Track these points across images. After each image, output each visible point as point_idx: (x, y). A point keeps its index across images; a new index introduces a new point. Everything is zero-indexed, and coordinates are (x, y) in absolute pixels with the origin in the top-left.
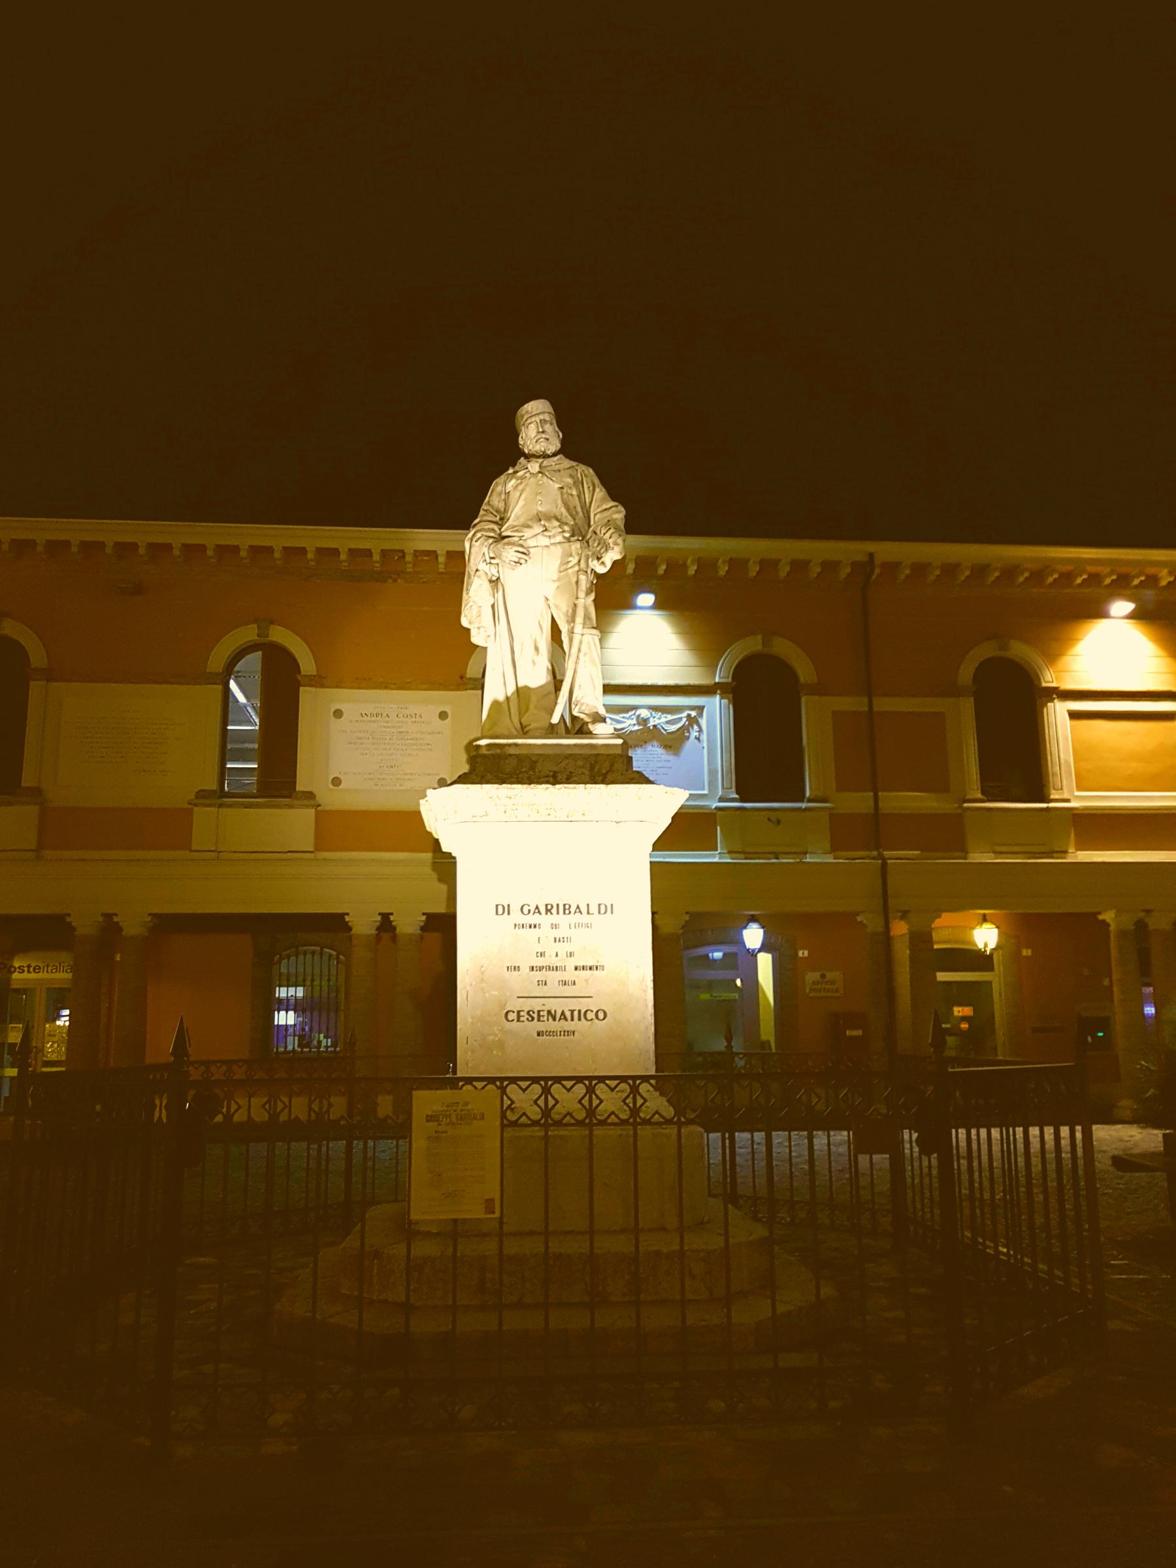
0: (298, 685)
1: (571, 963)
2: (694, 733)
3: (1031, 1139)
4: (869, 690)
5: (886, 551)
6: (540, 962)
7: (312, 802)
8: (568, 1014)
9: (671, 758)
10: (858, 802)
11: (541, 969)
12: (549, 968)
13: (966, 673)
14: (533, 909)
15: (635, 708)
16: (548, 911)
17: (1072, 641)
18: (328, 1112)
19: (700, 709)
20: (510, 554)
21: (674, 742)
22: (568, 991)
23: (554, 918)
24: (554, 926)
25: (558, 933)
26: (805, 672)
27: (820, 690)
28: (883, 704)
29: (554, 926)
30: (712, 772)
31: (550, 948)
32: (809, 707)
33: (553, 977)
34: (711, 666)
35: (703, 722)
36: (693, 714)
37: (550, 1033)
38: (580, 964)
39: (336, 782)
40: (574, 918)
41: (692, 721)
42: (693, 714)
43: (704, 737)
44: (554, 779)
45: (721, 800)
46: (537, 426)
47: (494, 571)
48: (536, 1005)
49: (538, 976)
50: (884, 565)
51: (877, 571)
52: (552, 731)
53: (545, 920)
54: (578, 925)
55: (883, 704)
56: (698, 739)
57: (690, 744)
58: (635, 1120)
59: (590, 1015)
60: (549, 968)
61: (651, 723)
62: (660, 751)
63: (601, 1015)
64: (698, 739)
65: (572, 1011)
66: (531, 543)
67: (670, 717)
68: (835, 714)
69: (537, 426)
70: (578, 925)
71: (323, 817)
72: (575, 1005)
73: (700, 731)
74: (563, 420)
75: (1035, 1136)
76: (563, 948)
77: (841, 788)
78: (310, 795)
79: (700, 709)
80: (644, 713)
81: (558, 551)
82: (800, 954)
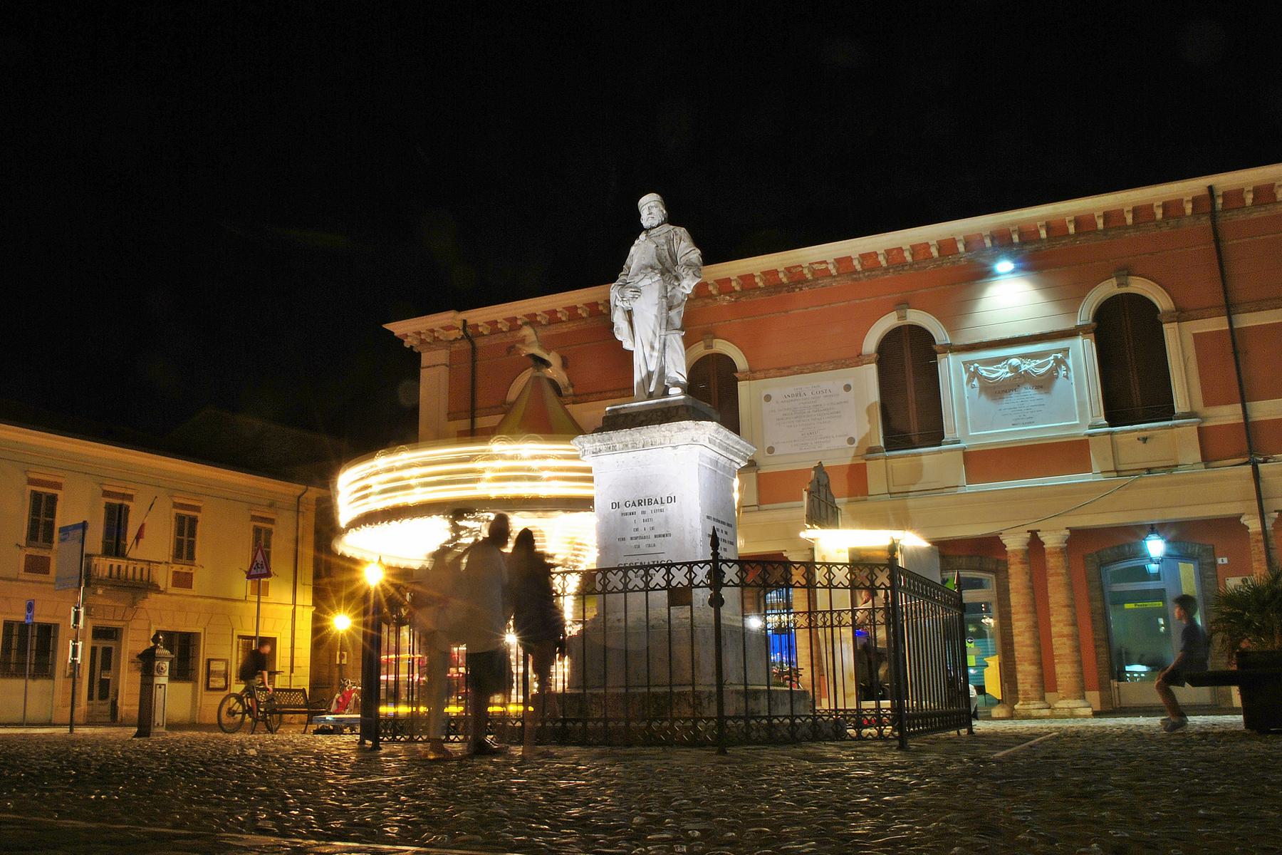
0: (737, 380)
1: (652, 534)
2: (1062, 373)
4: (1230, 309)
5: (1225, 181)
6: (636, 534)
9: (1044, 396)
10: (1228, 414)
12: (641, 538)
15: (1007, 358)
17: (982, 290)
19: (1066, 350)
20: (629, 294)
21: (1044, 383)
22: (652, 550)
23: (643, 508)
24: (643, 513)
25: (645, 517)
26: (1162, 301)
27: (1181, 314)
28: (1247, 320)
29: (643, 513)
30: (1081, 404)
31: (642, 526)
32: (1170, 332)
33: (643, 543)
34: (1073, 311)
35: (1070, 362)
36: (1060, 355)
39: (771, 450)
41: (1059, 362)
42: (1060, 355)
43: (1072, 374)
44: (641, 424)
45: (1091, 427)
46: (650, 208)
47: (626, 305)
49: (634, 542)
50: (1226, 195)
51: (1220, 201)
52: (651, 396)
53: (639, 509)
55: (1247, 320)
56: (1066, 377)
57: (1059, 383)
60: (641, 538)
61: (1023, 368)
62: (1032, 392)
64: (1066, 377)
66: (641, 284)
67: (1039, 362)
68: (1197, 337)
69: (650, 208)
70: (656, 511)
73: (1068, 369)
74: (668, 203)
75: (1021, 634)
77: (1209, 402)
79: (1066, 350)
80: (1015, 362)
81: (657, 286)
82: (1220, 561)
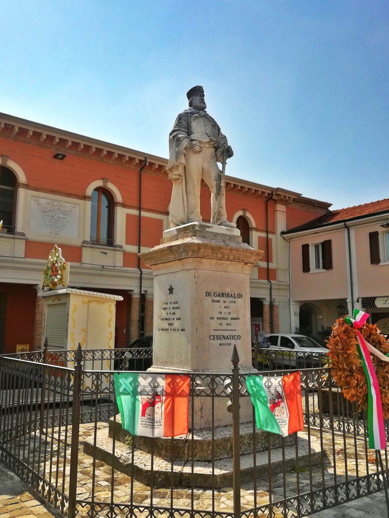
1: (229, 317)
3: (46, 474)
4: (140, 209)
7: (122, 249)
8: (229, 337)
11: (220, 318)
13: (90, 190)
14: (218, 294)
16: (223, 296)
18: (101, 385)
24: (224, 302)
25: (225, 305)
26: (22, 177)
28: (144, 214)
29: (224, 302)
33: (224, 322)
37: (224, 344)
38: (232, 317)
40: (231, 299)
48: (219, 333)
49: (220, 321)
53: (222, 299)
54: (231, 302)
55: (144, 214)
58: (213, 394)
59: (236, 337)
63: (239, 338)
65: (230, 336)
70: (231, 302)
71: (28, 242)
72: (231, 333)
76: (227, 310)
78: (23, 234)
